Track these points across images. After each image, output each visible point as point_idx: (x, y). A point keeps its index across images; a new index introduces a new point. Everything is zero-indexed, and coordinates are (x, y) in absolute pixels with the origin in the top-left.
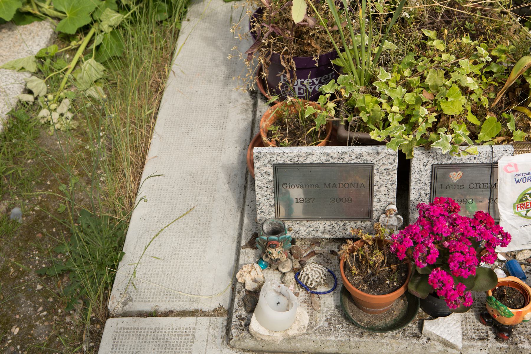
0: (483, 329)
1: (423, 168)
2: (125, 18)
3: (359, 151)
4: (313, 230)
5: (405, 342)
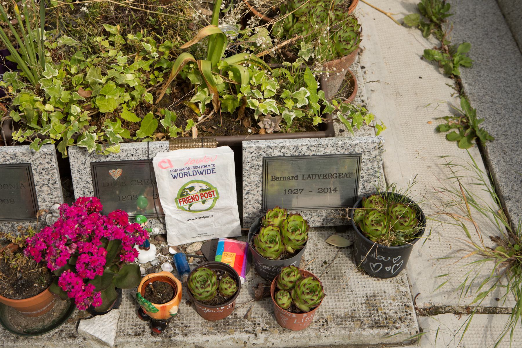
0: (140, 325)
1: (82, 167)
3: (12, 151)
5: (60, 343)
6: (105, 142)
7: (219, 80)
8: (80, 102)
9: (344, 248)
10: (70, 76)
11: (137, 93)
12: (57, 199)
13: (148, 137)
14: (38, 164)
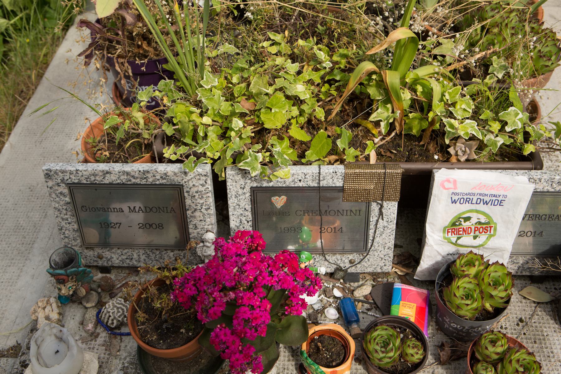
1: (240, 192)
2: (12, 25)
3: (163, 170)
4: (127, 259)
6: (271, 163)
7: (407, 95)
8: (242, 115)
9: (543, 303)
10: (231, 85)
11: (308, 107)
12: (210, 227)
13: (319, 160)
14: (191, 185)
